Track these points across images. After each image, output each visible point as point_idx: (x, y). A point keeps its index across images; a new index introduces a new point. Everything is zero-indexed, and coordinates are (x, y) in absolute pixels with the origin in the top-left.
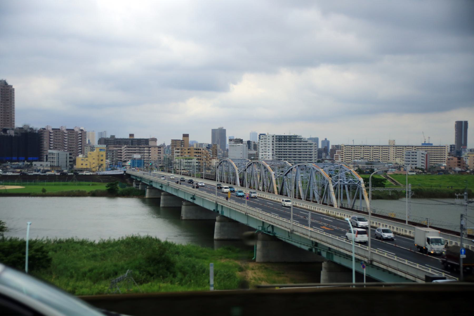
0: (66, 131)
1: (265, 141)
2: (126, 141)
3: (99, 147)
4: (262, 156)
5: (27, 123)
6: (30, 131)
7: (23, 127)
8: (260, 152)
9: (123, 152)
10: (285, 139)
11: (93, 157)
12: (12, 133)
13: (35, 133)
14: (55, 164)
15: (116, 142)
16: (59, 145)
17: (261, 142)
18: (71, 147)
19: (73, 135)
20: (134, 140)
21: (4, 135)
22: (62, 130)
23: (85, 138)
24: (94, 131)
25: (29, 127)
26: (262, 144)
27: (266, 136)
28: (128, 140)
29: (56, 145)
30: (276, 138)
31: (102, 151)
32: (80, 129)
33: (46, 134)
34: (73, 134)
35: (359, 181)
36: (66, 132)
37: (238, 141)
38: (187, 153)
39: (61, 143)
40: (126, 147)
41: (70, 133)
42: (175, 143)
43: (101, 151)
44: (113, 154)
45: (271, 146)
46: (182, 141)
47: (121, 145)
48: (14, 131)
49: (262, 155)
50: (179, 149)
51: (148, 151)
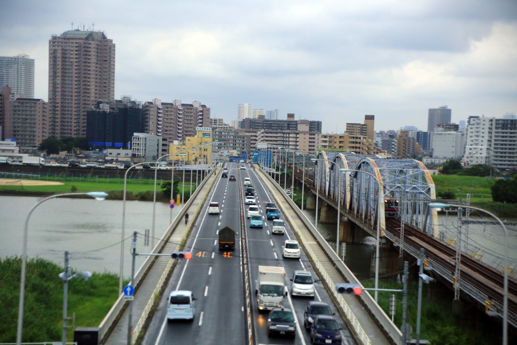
1: (477, 128)
4: (471, 151)
5: (127, 94)
6: (131, 105)
7: (123, 100)
8: (467, 144)
10: (512, 125)
12: (107, 108)
13: (139, 109)
14: (141, 153)
15: (266, 125)
16: (171, 127)
17: (471, 128)
18: (187, 130)
19: (191, 112)
20: (291, 123)
21: (95, 110)
24: (262, 109)
25: (130, 100)
26: (472, 132)
27: (480, 119)
28: (283, 123)
29: (167, 126)
30: (497, 124)
31: (206, 136)
32: (201, 104)
35: (428, 188)
36: (181, 108)
37: (452, 127)
38: (338, 142)
39: (173, 124)
40: (263, 132)
41: (186, 110)
42: (351, 128)
44: (244, 141)
45: (486, 135)
46: (363, 125)
47: (257, 129)
48: (108, 105)
49: (471, 149)
51: (294, 139)
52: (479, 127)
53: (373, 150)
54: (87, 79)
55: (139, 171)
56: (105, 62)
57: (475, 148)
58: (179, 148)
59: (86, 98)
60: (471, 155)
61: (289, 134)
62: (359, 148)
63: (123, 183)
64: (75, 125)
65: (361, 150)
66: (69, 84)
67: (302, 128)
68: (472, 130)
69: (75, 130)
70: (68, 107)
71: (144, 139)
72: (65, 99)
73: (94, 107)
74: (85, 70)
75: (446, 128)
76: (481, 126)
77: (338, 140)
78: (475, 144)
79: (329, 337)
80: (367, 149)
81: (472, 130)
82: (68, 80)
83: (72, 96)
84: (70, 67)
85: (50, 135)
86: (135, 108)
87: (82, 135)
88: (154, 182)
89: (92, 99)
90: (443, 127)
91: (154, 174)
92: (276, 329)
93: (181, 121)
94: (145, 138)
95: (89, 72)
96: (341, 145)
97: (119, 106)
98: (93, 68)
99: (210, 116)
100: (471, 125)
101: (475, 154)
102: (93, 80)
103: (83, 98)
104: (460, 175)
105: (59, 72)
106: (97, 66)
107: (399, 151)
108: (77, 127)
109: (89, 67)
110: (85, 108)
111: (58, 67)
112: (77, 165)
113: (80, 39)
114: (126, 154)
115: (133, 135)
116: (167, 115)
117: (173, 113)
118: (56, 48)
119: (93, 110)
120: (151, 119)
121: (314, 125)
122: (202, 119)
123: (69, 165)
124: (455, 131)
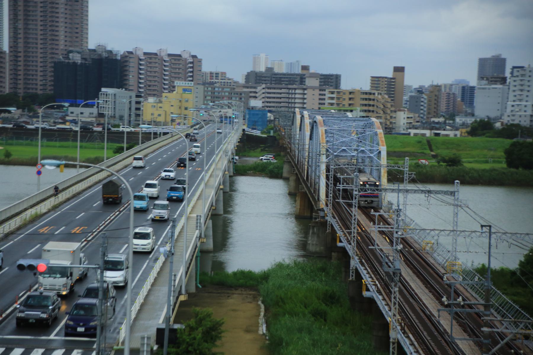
0: (167, 57)
1: (521, 80)
2: (292, 79)
3: (181, 85)
4: (513, 108)
5: (102, 43)
6: (107, 56)
7: (97, 49)
9: (259, 96)
11: (170, 102)
12: (78, 58)
13: (116, 60)
15: (274, 79)
16: (155, 81)
17: (515, 81)
19: (179, 64)
22: (160, 55)
23: (198, 70)
25: (105, 49)
26: (515, 86)
27: (525, 70)
28: (295, 76)
29: (150, 81)
31: (187, 92)
33: (132, 62)
34: (179, 62)
36: (166, 59)
37: (498, 80)
38: (347, 99)
41: (173, 61)
42: (376, 82)
43: (185, 93)
46: (391, 79)
48: (80, 55)
49: (513, 106)
50: (334, 92)
51: (301, 96)
52: (524, 80)
53: (389, 109)
54: (54, 23)
55: (95, 134)
57: (518, 105)
58: (154, 106)
59: (54, 46)
60: (513, 113)
61: (295, 89)
62: (373, 106)
63: (76, 147)
64: (42, 78)
65: (375, 108)
66: (33, 29)
67: (310, 82)
68: (515, 83)
69: (41, 85)
70: (33, 57)
71: (113, 95)
72: (29, 48)
73: (63, 57)
74: (52, 12)
75: (491, 81)
76: (527, 78)
77: (347, 96)
78: (519, 100)
79: (81, 324)
80: (382, 107)
81: (515, 83)
82: (32, 24)
83: (37, 44)
84: (35, 9)
85: (12, 91)
86: (112, 59)
87: (50, 90)
88: (104, 145)
89: (62, 47)
90: (487, 79)
91: (124, 137)
92: (24, 317)
93: (143, 73)
94: (115, 95)
95: (57, 15)
96: (351, 102)
97: (92, 56)
98: (62, 10)
99: (201, 68)
100: (515, 77)
101: (517, 111)
102: (62, 24)
103: (50, 47)
104: (490, 137)
105: (20, 15)
107: (429, 109)
108: (44, 81)
109: (57, 8)
110: (52, 58)
111: (19, 8)
112: (89, 129)
114: (90, 114)
115: (100, 90)
116: (151, 67)
117: (157, 65)
119: (61, 61)
120: (131, 72)
121: (331, 79)
122: (192, 72)
123: (14, 126)
124: (501, 84)
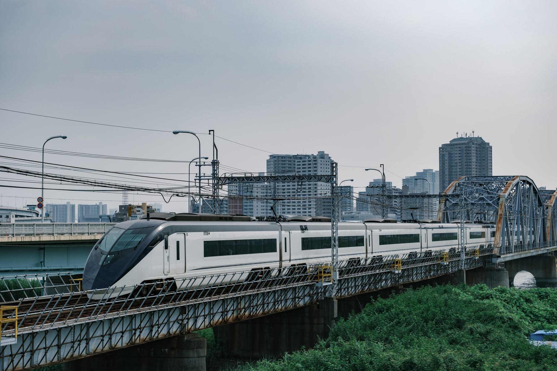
56: (484, 161)
98: (474, 167)
106: (477, 164)
113: (462, 144)
118: (445, 153)
